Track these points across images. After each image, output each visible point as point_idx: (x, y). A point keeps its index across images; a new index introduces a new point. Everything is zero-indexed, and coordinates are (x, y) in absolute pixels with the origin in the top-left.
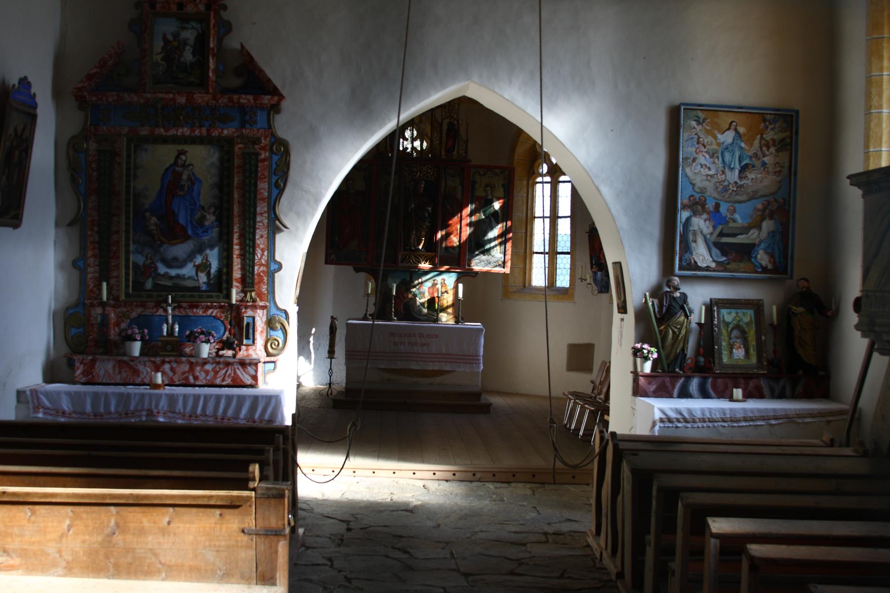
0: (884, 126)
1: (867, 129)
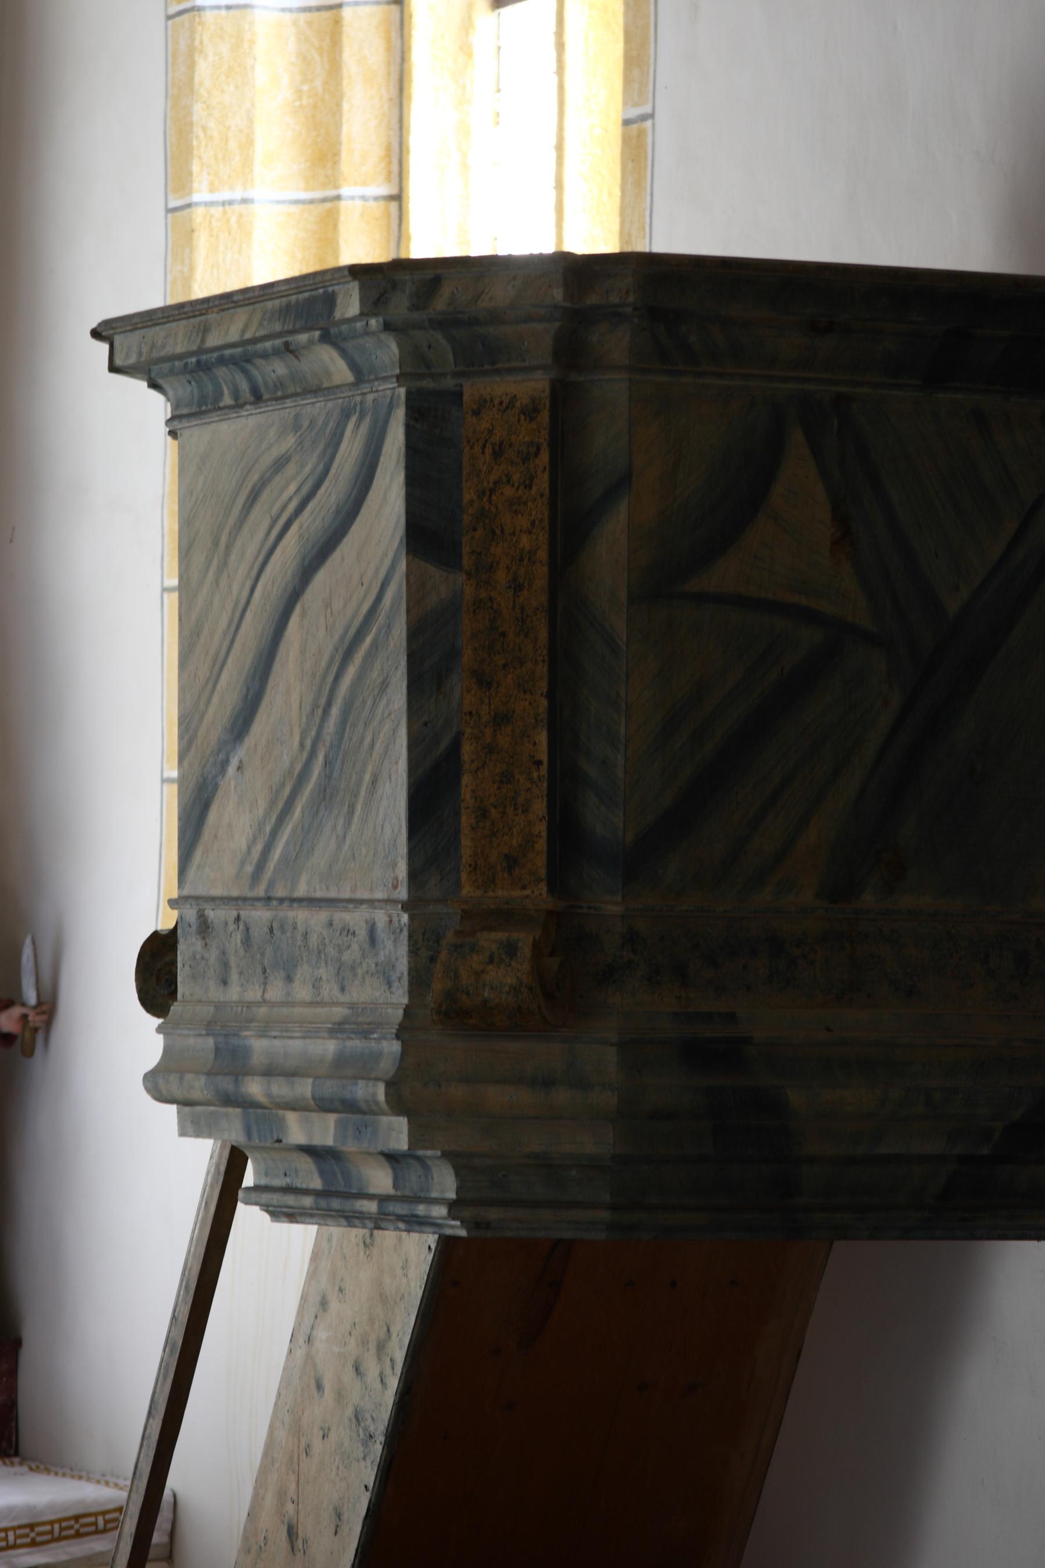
0: (261, 75)
1: (180, 93)
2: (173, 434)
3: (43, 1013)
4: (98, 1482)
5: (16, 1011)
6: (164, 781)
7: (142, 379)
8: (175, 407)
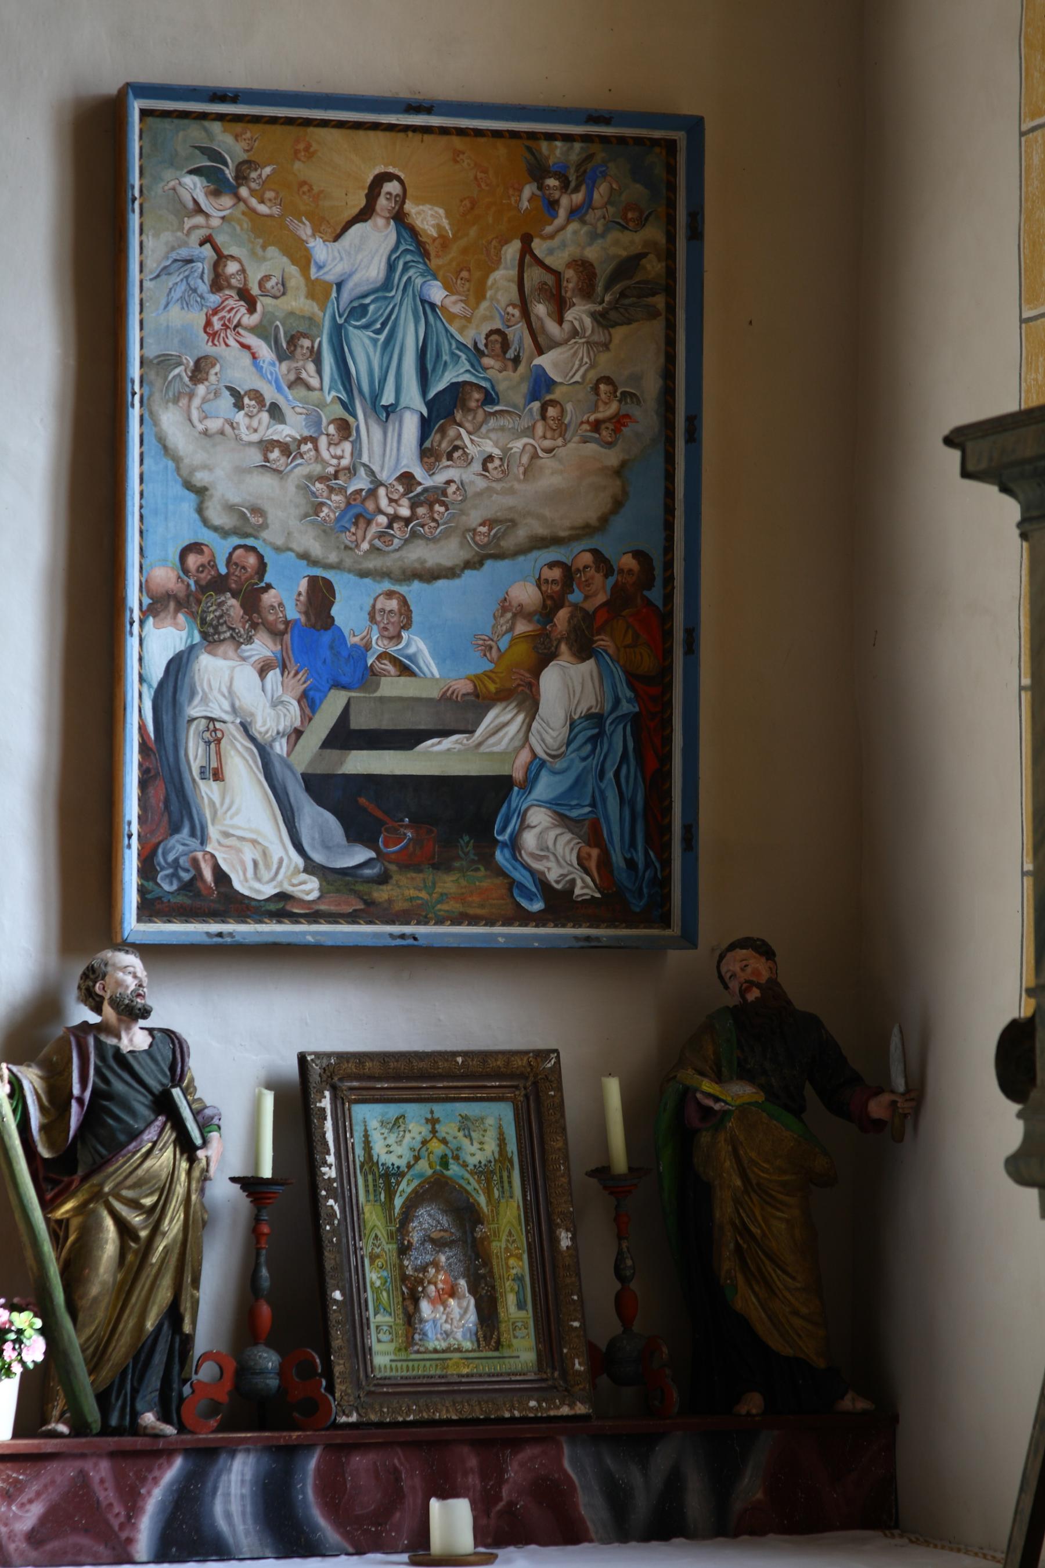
2: (1024, 536)
3: (912, 1100)
4: (976, 1555)
5: (886, 1098)
6: (1024, 874)
7: (992, 483)
8: (1025, 510)
